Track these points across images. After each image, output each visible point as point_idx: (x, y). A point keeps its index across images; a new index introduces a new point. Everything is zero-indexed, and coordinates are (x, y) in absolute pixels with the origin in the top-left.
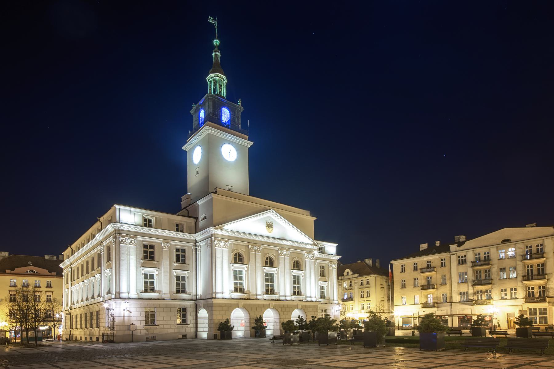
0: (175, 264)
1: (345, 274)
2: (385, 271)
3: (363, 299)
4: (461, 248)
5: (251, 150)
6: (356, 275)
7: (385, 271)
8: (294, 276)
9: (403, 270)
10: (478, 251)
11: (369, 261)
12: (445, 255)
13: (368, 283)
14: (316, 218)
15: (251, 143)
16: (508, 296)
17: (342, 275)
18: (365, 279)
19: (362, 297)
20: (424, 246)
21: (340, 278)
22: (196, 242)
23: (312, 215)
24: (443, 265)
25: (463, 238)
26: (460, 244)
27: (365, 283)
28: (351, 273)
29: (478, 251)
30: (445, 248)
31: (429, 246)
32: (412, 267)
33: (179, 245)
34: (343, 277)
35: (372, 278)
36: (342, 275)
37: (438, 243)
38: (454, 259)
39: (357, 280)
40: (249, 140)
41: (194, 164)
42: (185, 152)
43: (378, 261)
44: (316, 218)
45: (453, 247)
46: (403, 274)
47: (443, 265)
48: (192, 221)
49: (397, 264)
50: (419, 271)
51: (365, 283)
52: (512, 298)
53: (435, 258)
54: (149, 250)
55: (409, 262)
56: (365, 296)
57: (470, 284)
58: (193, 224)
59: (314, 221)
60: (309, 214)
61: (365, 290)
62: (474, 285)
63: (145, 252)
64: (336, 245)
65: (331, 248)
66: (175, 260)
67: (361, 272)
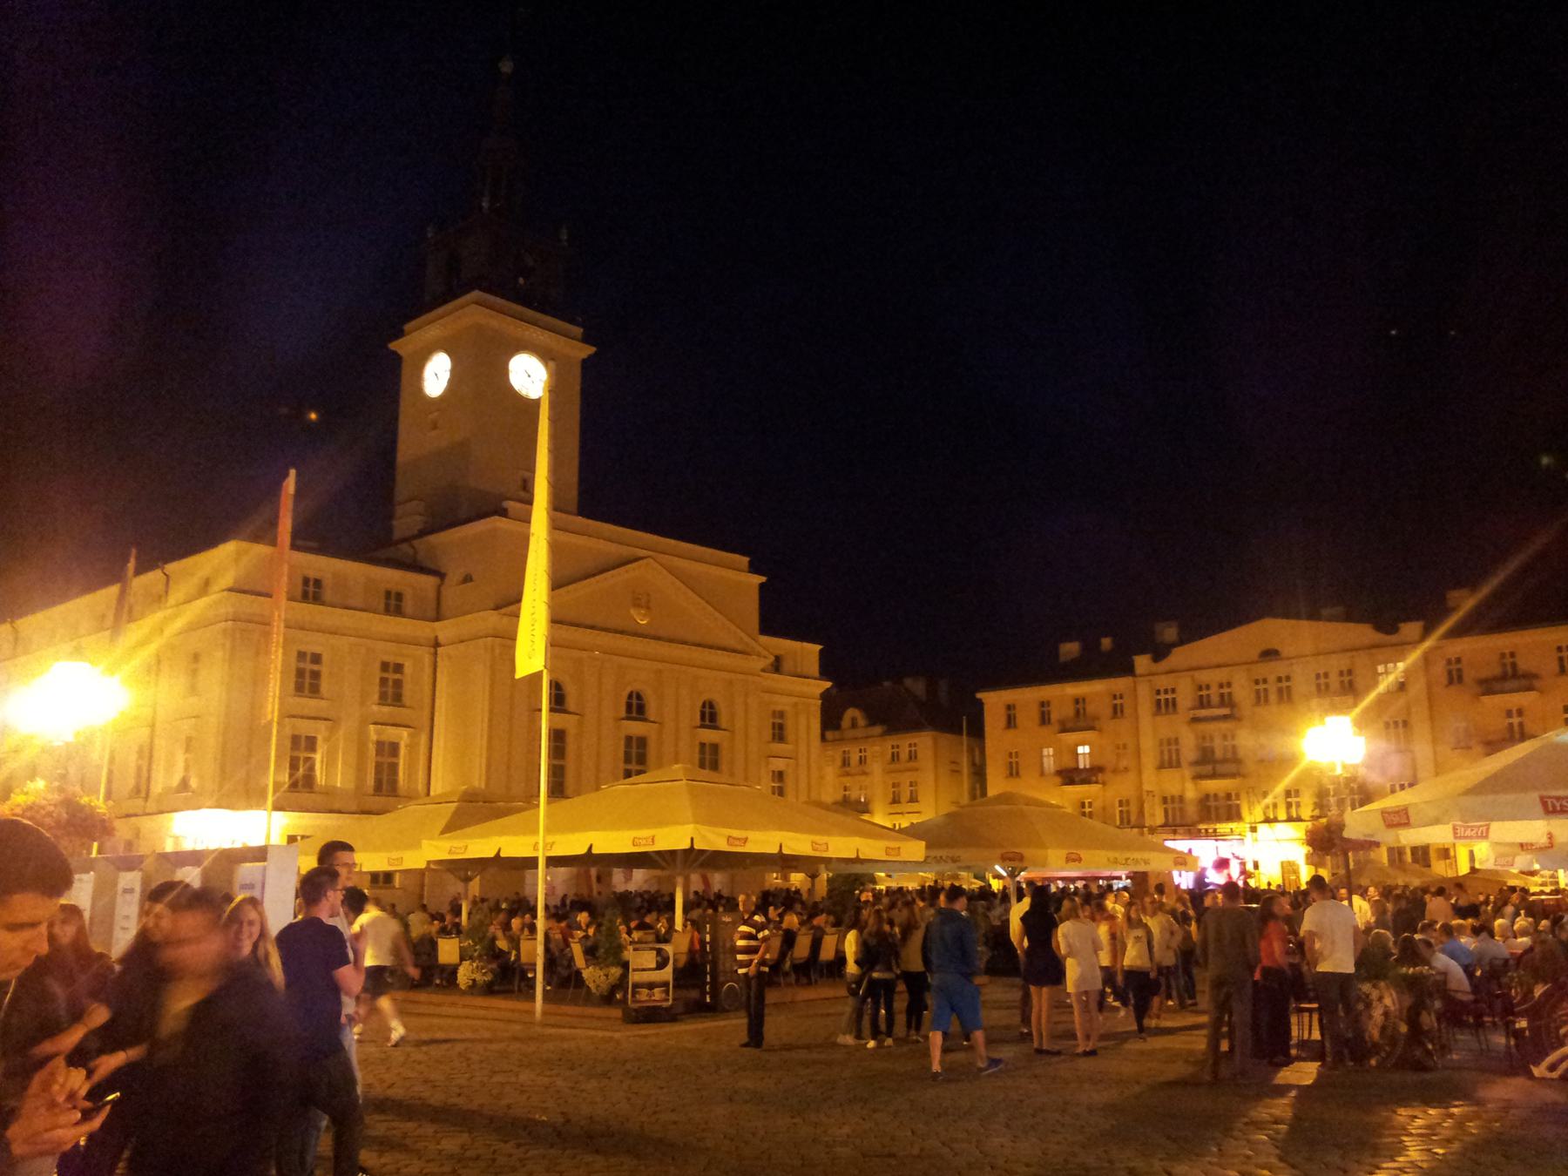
0: (375, 708)
1: (846, 722)
2: (961, 720)
3: (897, 808)
4: (1164, 665)
5: (586, 364)
6: (878, 729)
7: (961, 720)
8: (703, 745)
9: (1011, 722)
10: (1204, 677)
11: (917, 686)
12: (1120, 684)
13: (913, 757)
14: (763, 579)
15: (588, 351)
16: (1282, 815)
17: (838, 727)
18: (905, 742)
19: (895, 800)
20: (1070, 649)
21: (829, 735)
22: (437, 644)
23: (754, 568)
24: (1117, 712)
25: (1170, 633)
26: (1160, 653)
27: (904, 755)
28: (861, 722)
29: (1204, 677)
30: (1120, 666)
31: (1085, 648)
32: (1035, 714)
33: (390, 653)
34: (837, 734)
35: (924, 742)
36: (838, 727)
37: (1106, 643)
38: (1144, 691)
39: (879, 749)
40: (586, 340)
41: (420, 389)
42: (397, 359)
43: (943, 686)
44: (763, 579)
45: (1142, 662)
46: (1011, 732)
47: (1117, 712)
48: (427, 582)
49: (994, 701)
50: (1056, 727)
51: (904, 755)
52: (1290, 819)
53: (1094, 690)
54: (309, 666)
55: (1027, 697)
56: (905, 796)
57: (1188, 772)
58: (432, 595)
59: (762, 586)
60: (750, 607)
61: (905, 779)
62: (1198, 777)
63: (300, 673)
64: (817, 648)
65: (809, 653)
66: (376, 697)
67: (892, 718)
